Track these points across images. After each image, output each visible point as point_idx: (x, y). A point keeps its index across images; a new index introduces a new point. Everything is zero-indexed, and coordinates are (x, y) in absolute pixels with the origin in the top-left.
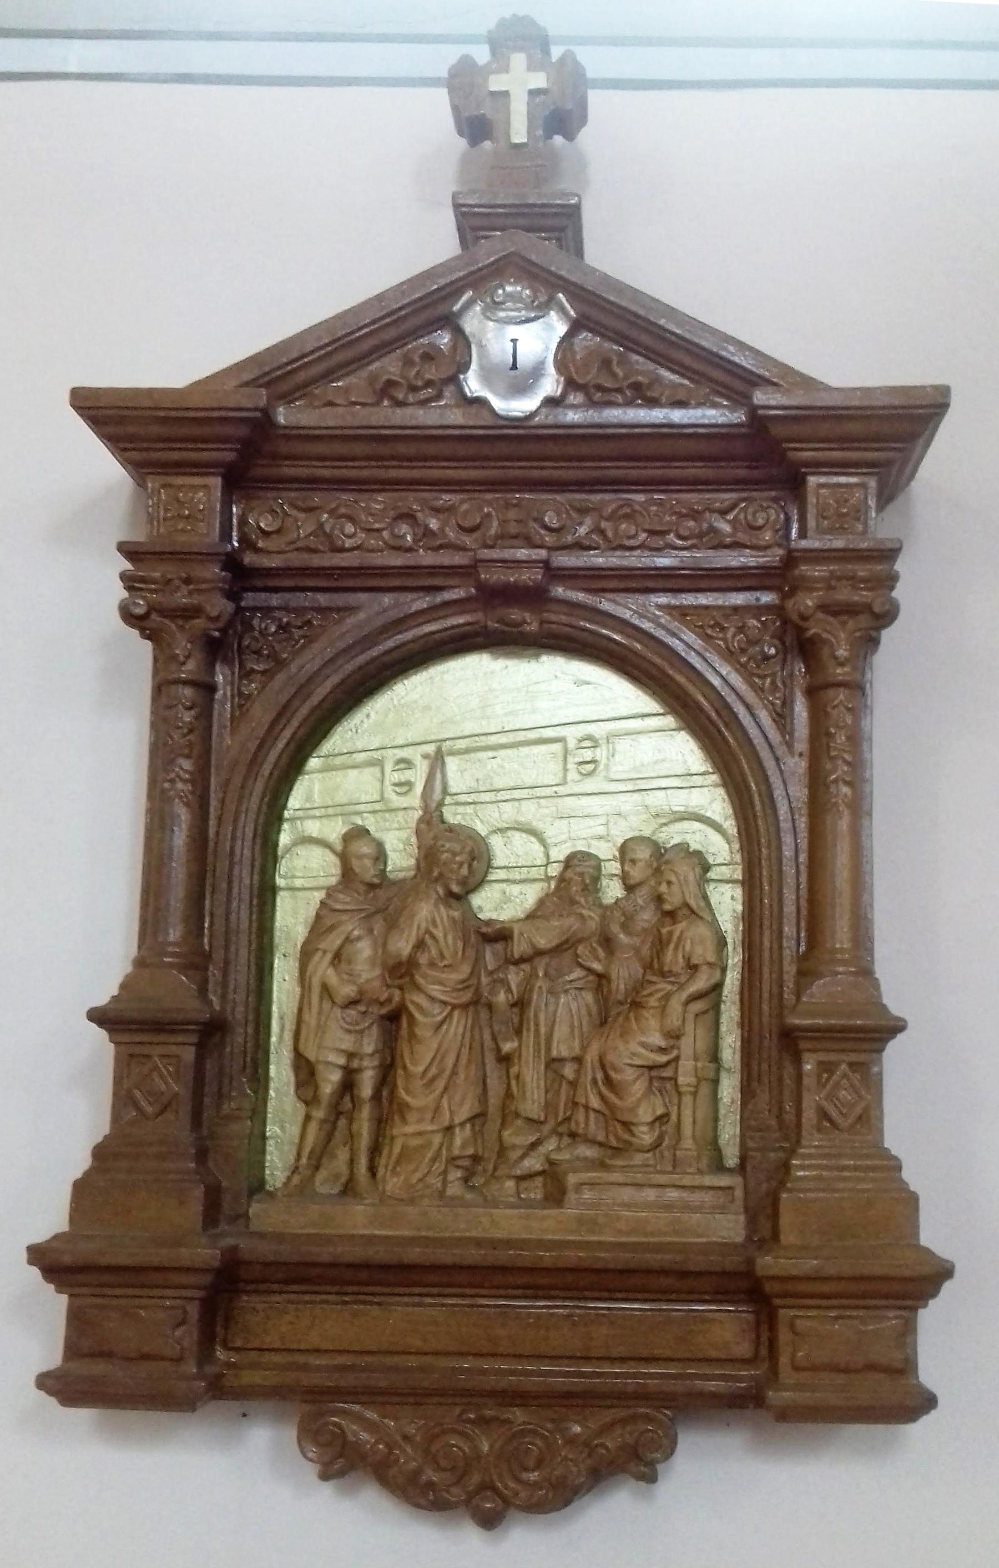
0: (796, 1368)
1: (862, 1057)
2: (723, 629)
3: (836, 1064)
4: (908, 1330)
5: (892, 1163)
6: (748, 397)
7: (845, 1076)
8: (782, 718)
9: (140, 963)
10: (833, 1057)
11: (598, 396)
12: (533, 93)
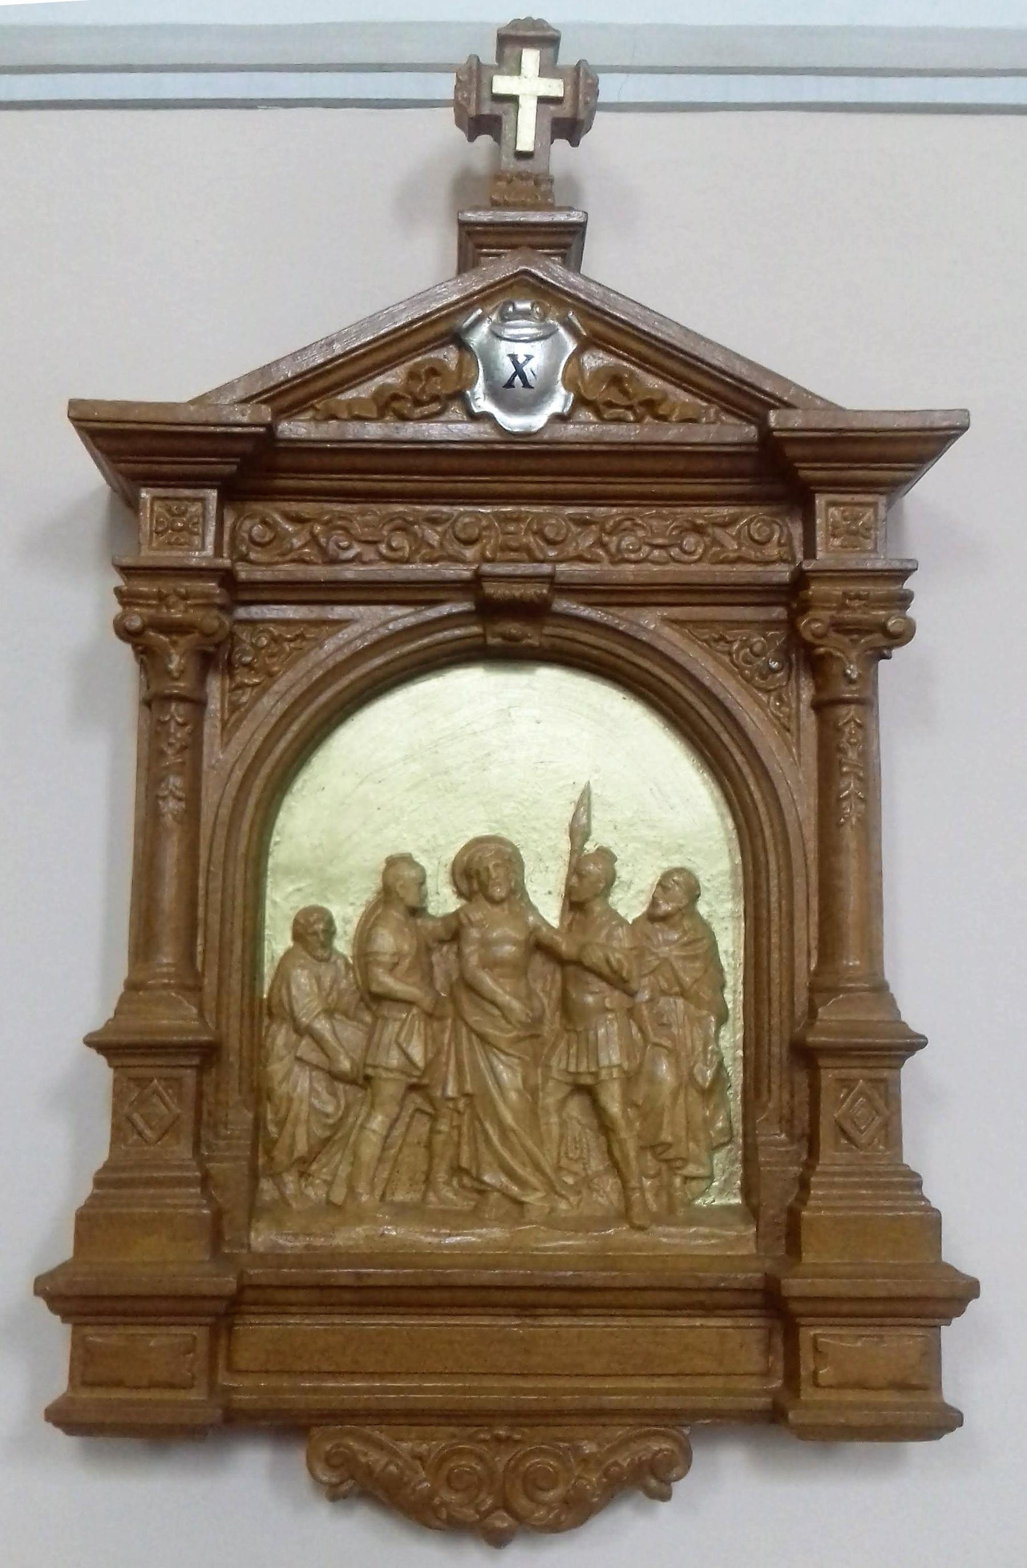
0: (817, 1385)
3: (856, 1080)
5: (915, 1180)
7: (861, 1093)
10: (844, 1073)
12: (543, 101)
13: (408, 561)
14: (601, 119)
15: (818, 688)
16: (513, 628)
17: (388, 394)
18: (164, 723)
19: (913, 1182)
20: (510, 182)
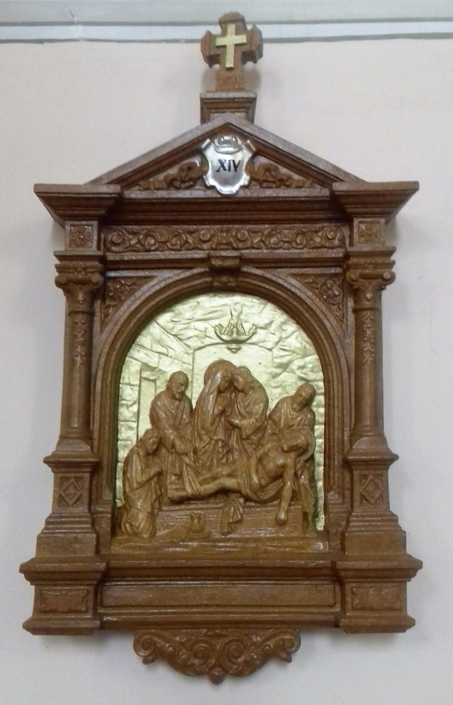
1: (379, 472)
2: (317, 284)
4: (404, 590)
6: (331, 185)
8: (342, 320)
9: (63, 438)
11: (265, 185)
12: (237, 45)
13: (179, 250)
14: (267, 48)
15: (355, 302)
16: (224, 279)
17: (170, 179)
18: (77, 323)
19: (394, 519)
20: (224, 80)
